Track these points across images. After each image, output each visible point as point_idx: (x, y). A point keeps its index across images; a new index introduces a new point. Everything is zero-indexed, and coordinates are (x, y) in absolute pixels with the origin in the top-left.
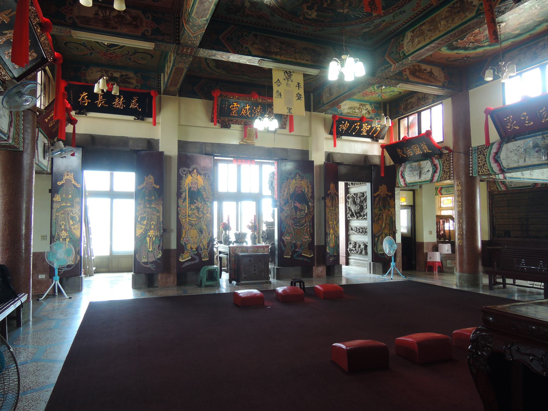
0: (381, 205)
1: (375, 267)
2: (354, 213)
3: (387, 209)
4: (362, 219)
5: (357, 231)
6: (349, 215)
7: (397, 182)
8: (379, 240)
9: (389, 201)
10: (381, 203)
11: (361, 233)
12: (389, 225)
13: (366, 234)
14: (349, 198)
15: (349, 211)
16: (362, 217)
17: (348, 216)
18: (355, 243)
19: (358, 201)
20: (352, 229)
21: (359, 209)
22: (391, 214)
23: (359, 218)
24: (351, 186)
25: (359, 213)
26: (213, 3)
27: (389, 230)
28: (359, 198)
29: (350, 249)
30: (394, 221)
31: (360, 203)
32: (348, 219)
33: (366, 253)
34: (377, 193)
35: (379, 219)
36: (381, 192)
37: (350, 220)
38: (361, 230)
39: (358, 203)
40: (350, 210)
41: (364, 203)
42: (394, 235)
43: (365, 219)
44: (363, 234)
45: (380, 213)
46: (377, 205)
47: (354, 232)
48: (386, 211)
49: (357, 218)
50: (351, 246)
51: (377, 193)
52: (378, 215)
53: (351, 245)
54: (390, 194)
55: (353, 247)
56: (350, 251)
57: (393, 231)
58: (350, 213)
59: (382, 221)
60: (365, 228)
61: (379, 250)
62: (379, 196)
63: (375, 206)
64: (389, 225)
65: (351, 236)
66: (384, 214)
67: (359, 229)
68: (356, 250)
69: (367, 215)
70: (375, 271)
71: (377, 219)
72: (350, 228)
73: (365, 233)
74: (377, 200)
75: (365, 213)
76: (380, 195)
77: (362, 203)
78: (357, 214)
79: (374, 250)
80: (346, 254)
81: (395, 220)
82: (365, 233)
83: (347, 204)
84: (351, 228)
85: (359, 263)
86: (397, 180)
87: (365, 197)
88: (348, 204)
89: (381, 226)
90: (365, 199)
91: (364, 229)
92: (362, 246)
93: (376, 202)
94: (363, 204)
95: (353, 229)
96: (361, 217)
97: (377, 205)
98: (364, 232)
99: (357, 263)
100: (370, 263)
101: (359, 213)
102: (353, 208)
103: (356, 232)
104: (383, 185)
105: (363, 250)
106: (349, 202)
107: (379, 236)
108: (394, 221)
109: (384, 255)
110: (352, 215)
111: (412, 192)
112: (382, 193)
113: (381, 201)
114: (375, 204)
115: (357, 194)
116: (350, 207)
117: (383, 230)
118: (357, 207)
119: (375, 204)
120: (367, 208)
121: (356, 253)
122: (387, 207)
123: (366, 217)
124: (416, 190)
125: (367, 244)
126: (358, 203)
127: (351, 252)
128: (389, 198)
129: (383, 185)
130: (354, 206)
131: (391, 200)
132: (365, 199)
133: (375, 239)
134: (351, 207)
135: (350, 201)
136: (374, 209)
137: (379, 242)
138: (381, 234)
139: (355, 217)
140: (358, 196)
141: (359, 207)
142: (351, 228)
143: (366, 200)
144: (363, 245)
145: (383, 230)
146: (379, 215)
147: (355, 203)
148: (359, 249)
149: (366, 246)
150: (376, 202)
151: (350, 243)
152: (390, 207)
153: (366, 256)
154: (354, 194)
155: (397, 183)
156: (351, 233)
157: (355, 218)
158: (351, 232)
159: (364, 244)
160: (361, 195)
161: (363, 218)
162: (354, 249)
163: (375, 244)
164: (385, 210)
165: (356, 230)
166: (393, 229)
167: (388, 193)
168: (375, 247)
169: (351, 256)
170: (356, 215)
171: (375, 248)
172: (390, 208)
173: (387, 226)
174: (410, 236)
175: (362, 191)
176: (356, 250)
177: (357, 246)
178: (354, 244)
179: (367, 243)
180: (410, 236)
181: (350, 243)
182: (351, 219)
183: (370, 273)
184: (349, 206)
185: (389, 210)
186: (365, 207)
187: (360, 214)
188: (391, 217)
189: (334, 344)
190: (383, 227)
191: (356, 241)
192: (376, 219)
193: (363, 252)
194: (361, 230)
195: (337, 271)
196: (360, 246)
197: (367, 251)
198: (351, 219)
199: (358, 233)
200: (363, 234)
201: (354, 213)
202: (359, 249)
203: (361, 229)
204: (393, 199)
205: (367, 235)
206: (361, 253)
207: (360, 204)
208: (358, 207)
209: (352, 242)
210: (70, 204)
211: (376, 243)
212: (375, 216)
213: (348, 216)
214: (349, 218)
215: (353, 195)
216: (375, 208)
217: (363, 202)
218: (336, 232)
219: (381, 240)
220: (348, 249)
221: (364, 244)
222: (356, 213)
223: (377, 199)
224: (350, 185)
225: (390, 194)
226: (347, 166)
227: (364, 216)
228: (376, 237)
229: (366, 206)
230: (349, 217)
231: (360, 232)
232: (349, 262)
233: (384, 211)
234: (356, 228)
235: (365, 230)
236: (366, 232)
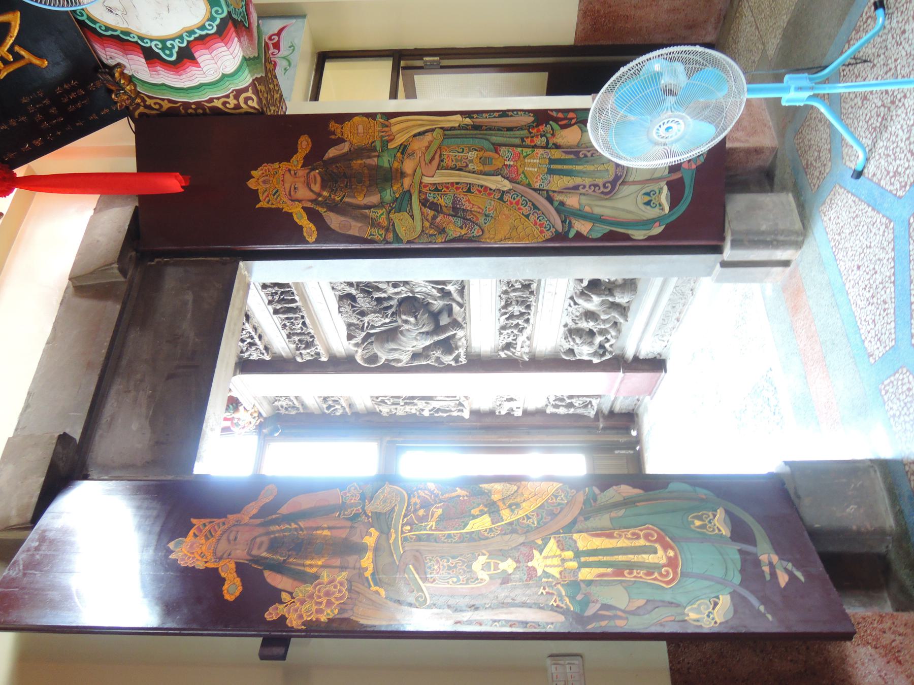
0: (374, 199)
1: (763, 233)
2: (436, 338)
3: (396, 165)
4: (461, 306)
5: (518, 325)
6: (448, 359)
7: (232, 102)
8: (587, 209)
9: (345, 148)
10: (361, 200)
11: (528, 307)
12: (497, 152)
13: (534, 287)
14: (373, 358)
15: (427, 357)
16: (455, 306)
17: (453, 364)
18: (573, 332)
19: (379, 321)
20: (508, 346)
21: (416, 317)
22: (428, 137)
23: (460, 319)
24: (320, 349)
25: (435, 316)
26: (6, 590)
27: (529, 151)
28: (366, 319)
29: (595, 354)
30: (468, 121)
31: (390, 312)
32: (463, 359)
33: (630, 285)
34: (302, 220)
35: (456, 210)
36: (293, 201)
37: (467, 354)
38: (516, 309)
39: (387, 320)
40: (424, 353)
41: (383, 295)
42: (556, 120)
43: (461, 291)
44: (532, 298)
45: (424, 203)
46: (375, 224)
47: (521, 339)
48: (408, 166)
49: (456, 324)
50: (584, 352)
51: (302, 220)
52: (431, 213)
53: (576, 351)
54: (304, 144)
55: (591, 344)
56: (603, 355)
57: (529, 127)
58: (438, 353)
59: (469, 191)
60: (505, 292)
61: (651, 213)
62: (322, 210)
63: (378, 234)
64: (497, 152)
65: (538, 350)
66: (426, 180)
67: (512, 316)
68: (602, 332)
69: (444, 283)
70: (782, 232)
71: (460, 222)
72: (503, 355)
73: (532, 293)
74: (342, 219)
75: (435, 292)
76: (312, 201)
77: (386, 304)
78: (442, 323)
79: (650, 238)
80: (616, 369)
81: (462, 113)
82: (532, 293)
83: (400, 365)
84: (503, 349)
85: (666, 317)
86: (218, 104)
87: (353, 291)
88: (398, 361)
89: (501, 199)
90: (368, 288)
91: (512, 294)
92: (595, 303)
93: (355, 228)
94: (390, 298)
95: (510, 340)
96: (456, 308)
97: (375, 224)
98: (525, 295)
99: (663, 325)
100: (724, 264)
101: (435, 316)
102: (415, 343)
103: (521, 330)
104: (252, 184)
105: (611, 299)
106: (391, 356)
107: (561, 208)
108: (468, 121)
109: (681, 181)
110: (447, 346)
111: (330, 68)
112: (303, 193)
113: (346, 200)
114: (368, 232)
115: (349, 325)
116: (410, 354)
117: (529, 186)
118: (406, 327)
119: (368, 232)
120: (406, 283)
121: (619, 331)
122: (386, 165)
123: (450, 288)
124: (315, 42)
125: (585, 283)
126: (387, 320)
127: (609, 349)
128: (332, 153)
129: (252, 184)
130: (402, 338)
131: (341, 141)
132: (363, 291)
133: (579, 236)
134: (408, 349)
135: (383, 357)
136: (398, 239)
137: (597, 211)
138: (550, 199)
139: (454, 335)
140: (355, 321)
141: (404, 317)
142: (503, 349)
143: (368, 285)
144: (588, 299)
145: (529, 186)
146: (435, 207)
147: (391, 335)
148: (603, 317)
149: (595, 286)
150: (355, 228)
151: (571, 351)
152: (385, 143)
153: (640, 286)
154: (350, 337)
155: (237, 97)
156: (526, 350)
157: (460, 333)
158: (521, 351)
159: (582, 294)
160: (348, 308)
161: (459, 299)
162: (599, 339)
163: (611, 232)
164: (403, 175)
165: (516, 331)
166: (521, 128)
167: (298, 159)
168: (627, 237)
169: (623, 349)
170: (445, 329)
171: (639, 235)
172: (391, 145)
173: (498, 164)
174: (546, 74)
175: (334, 303)
176: (602, 332)
177: (590, 325)
178: (578, 340)
179: (581, 281)
180: (546, 74)
181: (571, 351)
182: (462, 351)
183: (786, 264)
184: (405, 358)
185: (403, 149)
186: (404, 292)
187: (440, 312)
188: (446, 137)
189: (257, 206)
190: (506, 185)
191: (562, 330)
192: (454, 229)
193: (621, 298)
194: (516, 309)
195: (852, 509)
196: (590, 315)
197: (620, 282)
198: (462, 351)
199: (527, 321)
200: (532, 298)
201: (436, 338)
202: (603, 317)
203: (510, 309)
204: (333, 126)
205: (539, 281)
206: (623, 310)
207: (393, 314)
208: (406, 322)
209: (567, 346)
210: (372, 530)
211: (607, 229)
212: (442, 231)
213: (453, 364)
214: (458, 356)
215: (354, 341)
216: (390, 236)
217: (384, 299)
218: (553, 515)
219: (584, 200)
220: (596, 360)
221: (582, 294)
222: (438, 329)
223: (334, 221)
224: (318, 354)
225: (304, 144)
226: (110, 406)
227: (446, 294)
228: (571, 226)
229: (395, 285)
230: (456, 359)
231: (522, 314)
232: (651, 356)
233: (407, 182)
234: (503, 328)
235: (515, 290)
236: (526, 286)
